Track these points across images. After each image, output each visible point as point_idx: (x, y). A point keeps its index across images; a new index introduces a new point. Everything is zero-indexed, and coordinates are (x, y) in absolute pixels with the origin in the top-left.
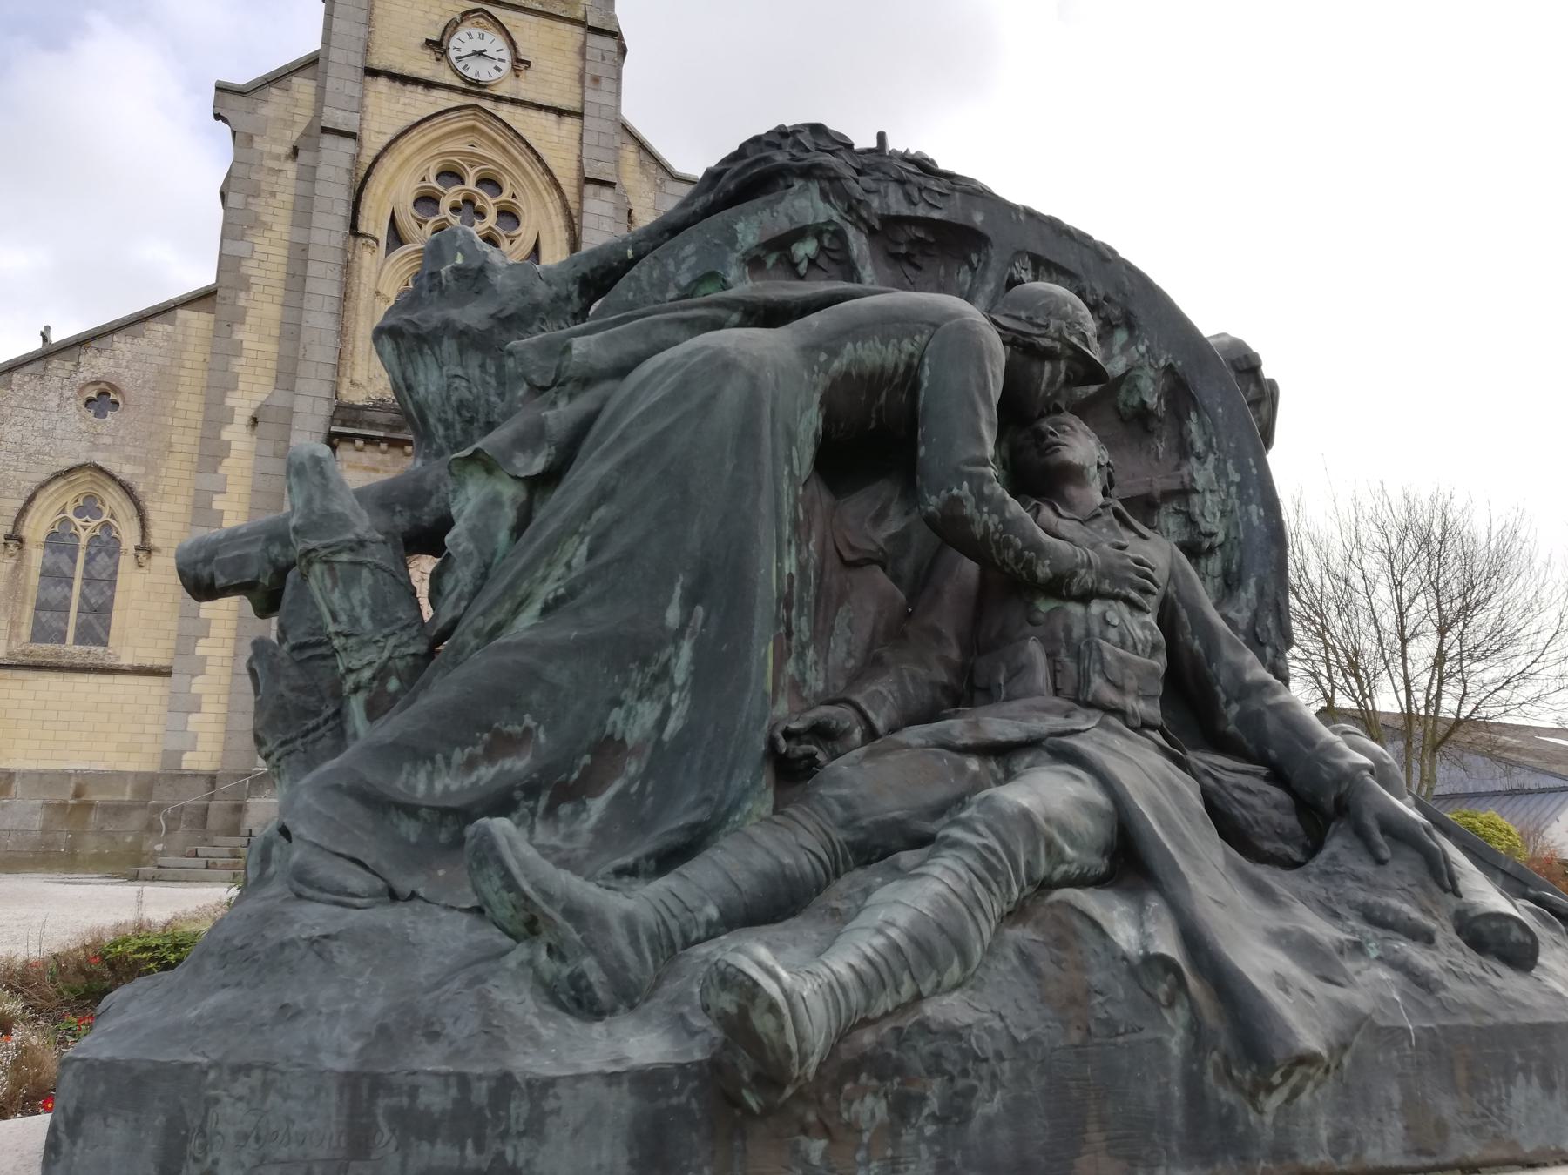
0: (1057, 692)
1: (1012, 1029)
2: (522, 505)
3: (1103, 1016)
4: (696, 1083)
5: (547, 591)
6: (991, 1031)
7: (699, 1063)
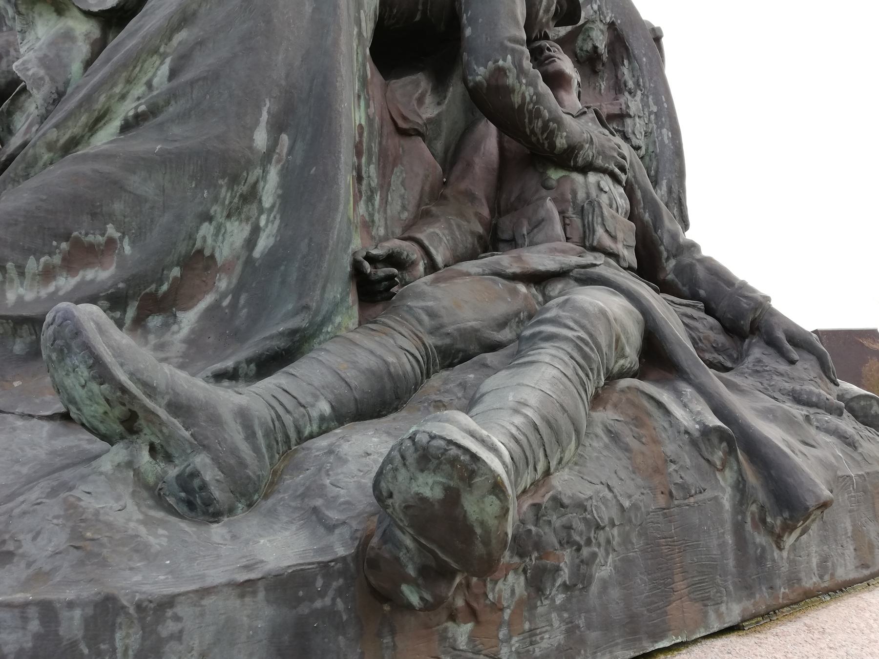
0: (568, 239)
1: (619, 498)
2: (96, 41)
3: (679, 481)
4: (341, 581)
5: (127, 109)
6: (604, 500)
7: (344, 559)
